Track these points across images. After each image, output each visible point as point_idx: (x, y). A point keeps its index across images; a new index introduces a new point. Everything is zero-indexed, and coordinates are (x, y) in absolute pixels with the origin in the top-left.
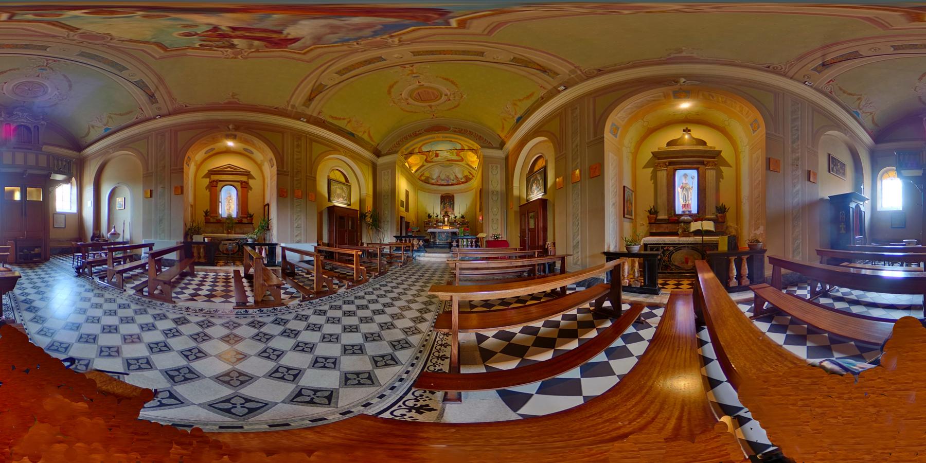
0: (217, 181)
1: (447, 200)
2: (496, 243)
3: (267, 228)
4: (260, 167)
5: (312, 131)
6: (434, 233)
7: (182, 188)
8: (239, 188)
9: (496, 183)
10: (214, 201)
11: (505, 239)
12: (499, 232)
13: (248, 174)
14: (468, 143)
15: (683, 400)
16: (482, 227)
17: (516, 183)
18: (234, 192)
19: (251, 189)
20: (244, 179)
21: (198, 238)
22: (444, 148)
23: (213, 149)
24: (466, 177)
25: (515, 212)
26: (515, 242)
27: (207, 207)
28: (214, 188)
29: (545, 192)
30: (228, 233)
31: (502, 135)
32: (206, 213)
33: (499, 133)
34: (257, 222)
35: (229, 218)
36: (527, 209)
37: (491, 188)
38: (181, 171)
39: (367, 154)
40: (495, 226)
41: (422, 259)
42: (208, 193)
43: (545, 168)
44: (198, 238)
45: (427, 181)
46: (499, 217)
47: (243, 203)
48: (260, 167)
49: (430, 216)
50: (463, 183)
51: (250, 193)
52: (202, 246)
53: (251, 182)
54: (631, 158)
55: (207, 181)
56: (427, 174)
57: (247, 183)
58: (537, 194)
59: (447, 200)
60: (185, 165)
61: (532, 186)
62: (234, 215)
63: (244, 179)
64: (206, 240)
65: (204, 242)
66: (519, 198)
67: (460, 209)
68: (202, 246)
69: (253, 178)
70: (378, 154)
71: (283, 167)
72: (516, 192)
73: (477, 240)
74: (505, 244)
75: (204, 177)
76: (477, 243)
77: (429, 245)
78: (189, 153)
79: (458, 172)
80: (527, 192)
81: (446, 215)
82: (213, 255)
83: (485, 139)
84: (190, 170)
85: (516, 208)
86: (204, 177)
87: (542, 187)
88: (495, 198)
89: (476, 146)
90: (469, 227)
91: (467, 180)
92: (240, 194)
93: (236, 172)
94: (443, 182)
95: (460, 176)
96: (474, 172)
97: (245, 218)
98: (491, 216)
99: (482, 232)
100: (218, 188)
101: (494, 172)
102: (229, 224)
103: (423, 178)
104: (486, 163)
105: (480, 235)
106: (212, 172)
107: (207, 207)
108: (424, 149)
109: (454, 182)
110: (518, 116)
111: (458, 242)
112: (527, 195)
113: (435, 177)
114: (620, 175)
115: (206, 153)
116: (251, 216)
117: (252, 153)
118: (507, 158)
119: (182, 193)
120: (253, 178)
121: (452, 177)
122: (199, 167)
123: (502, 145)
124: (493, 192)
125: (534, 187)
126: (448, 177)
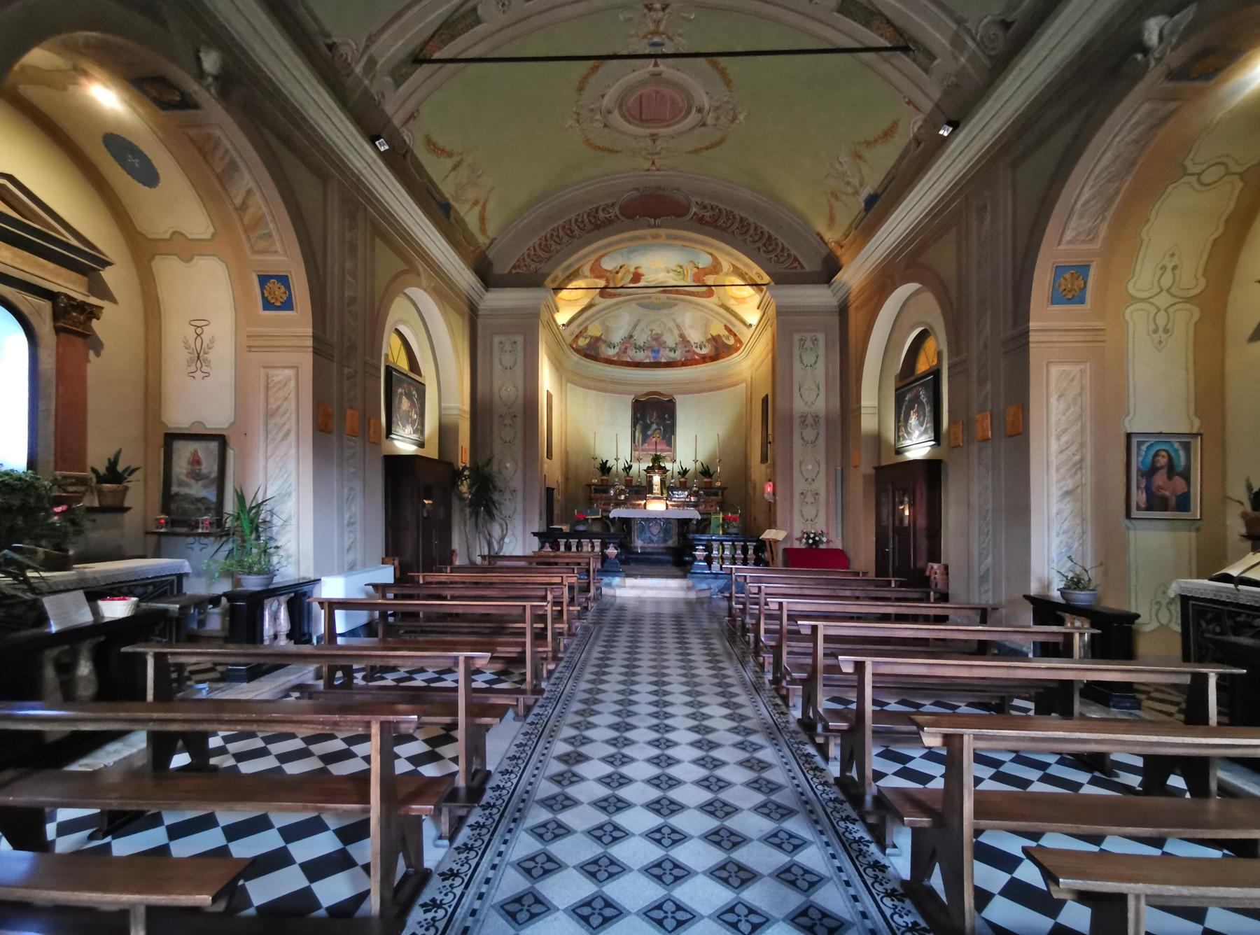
1: (654, 415)
2: (811, 558)
6: (626, 522)
9: (813, 394)
11: (837, 544)
12: (820, 526)
14: (729, 257)
16: (771, 508)
17: (868, 398)
22: (660, 263)
24: (715, 340)
25: (865, 476)
26: (864, 557)
29: (937, 438)
31: (831, 236)
33: (821, 227)
36: (897, 478)
37: (799, 406)
39: (464, 277)
40: (809, 512)
41: (620, 593)
43: (936, 373)
45: (591, 352)
46: (820, 485)
49: (605, 468)
50: (705, 359)
54: (1184, 319)
56: (595, 330)
58: (918, 447)
59: (654, 415)
61: (907, 417)
66: (878, 439)
67: (692, 446)
70: (487, 276)
71: (324, 331)
72: (868, 423)
73: (761, 546)
74: (837, 559)
76: (761, 554)
77: (634, 562)
79: (693, 324)
80: (898, 429)
81: (657, 465)
83: (790, 261)
85: (866, 467)
87: (929, 424)
88: (809, 434)
89: (755, 271)
90: (728, 505)
91: (720, 350)
92: (48, 362)
94: (641, 356)
95: (695, 336)
96: (745, 334)
98: (799, 486)
99: (772, 524)
101: (809, 359)
103: (582, 342)
104: (787, 326)
105: (768, 535)
108: (608, 264)
109: (678, 355)
110: (867, 191)
111: (708, 548)
112: (898, 438)
113: (617, 338)
114: (1108, 396)
118: (843, 310)
121: (670, 340)
123: (829, 270)
124: (804, 418)
125: (913, 420)
126: (657, 338)
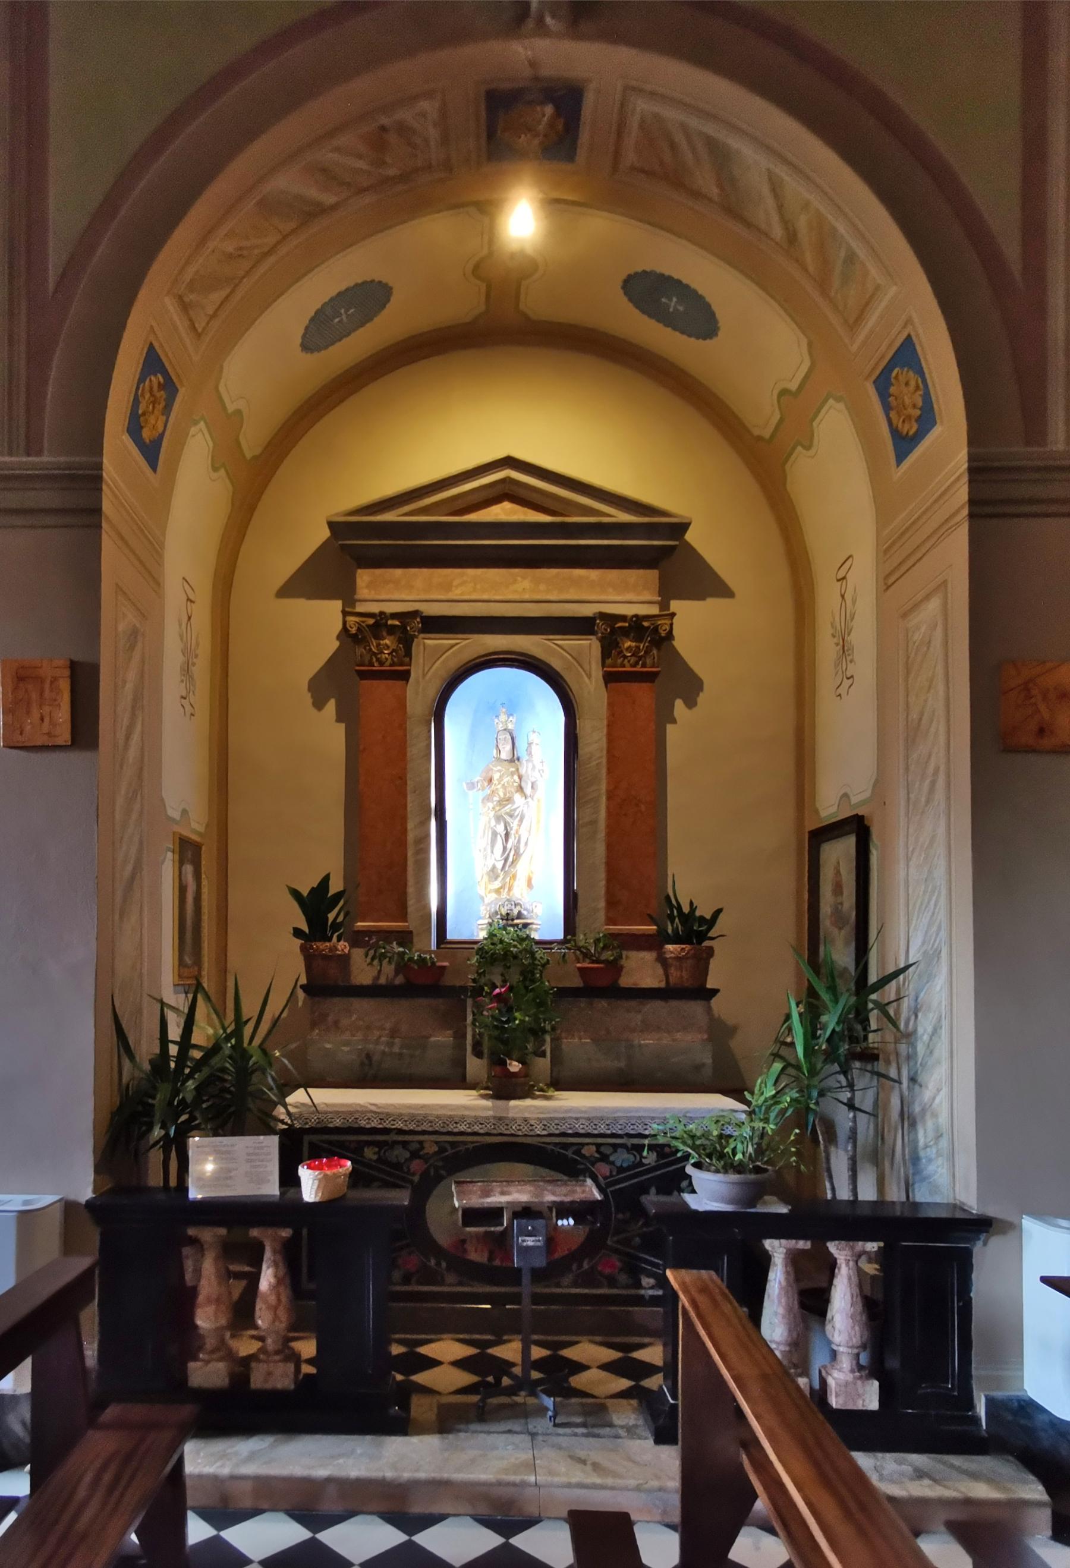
0: (410, 627)
3: (852, 1024)
4: (763, 461)
5: (669, 1105)
7: (84, 681)
8: (591, 687)
10: (391, 811)
13: (656, 546)
15: (789, 1345)
18: (543, 722)
19: (690, 687)
20: (626, 594)
21: (218, 1167)
23: (369, 298)
27: (323, 859)
28: (385, 690)
30: (505, 1088)
32: (316, 904)
34: (755, 980)
35: (508, 951)
38: (77, 501)
42: (327, 732)
44: (218, 1167)
47: (616, 813)
48: (763, 461)
51: (685, 731)
52: (271, 1239)
53: (692, 624)
55: (322, 623)
57: (653, 634)
60: (117, 450)
62: (546, 916)
63: (626, 594)
64: (310, 1185)
65: (286, 1209)
68: (271, 1239)
69: (705, 583)
75: (290, 589)
78: (152, 317)
82: (383, 1305)
84: (176, 515)
86: (290, 589)
93: (565, 529)
97: (628, 956)
100: (418, 693)
102: (508, 1003)
106: (367, 541)
107: (321, 856)
115: (320, 332)
116: (695, 930)
117: (702, 321)
119: (84, 732)
120: (705, 583)
122: (255, 479)
